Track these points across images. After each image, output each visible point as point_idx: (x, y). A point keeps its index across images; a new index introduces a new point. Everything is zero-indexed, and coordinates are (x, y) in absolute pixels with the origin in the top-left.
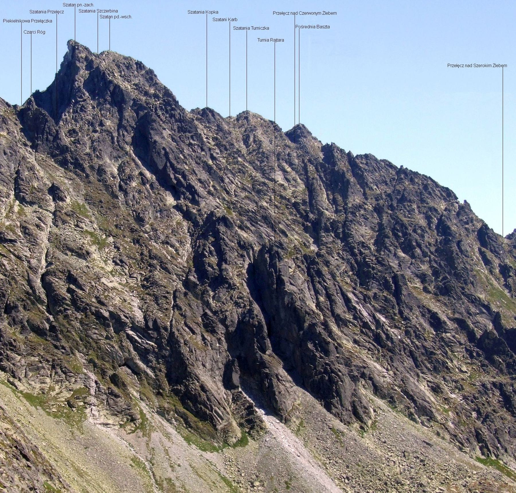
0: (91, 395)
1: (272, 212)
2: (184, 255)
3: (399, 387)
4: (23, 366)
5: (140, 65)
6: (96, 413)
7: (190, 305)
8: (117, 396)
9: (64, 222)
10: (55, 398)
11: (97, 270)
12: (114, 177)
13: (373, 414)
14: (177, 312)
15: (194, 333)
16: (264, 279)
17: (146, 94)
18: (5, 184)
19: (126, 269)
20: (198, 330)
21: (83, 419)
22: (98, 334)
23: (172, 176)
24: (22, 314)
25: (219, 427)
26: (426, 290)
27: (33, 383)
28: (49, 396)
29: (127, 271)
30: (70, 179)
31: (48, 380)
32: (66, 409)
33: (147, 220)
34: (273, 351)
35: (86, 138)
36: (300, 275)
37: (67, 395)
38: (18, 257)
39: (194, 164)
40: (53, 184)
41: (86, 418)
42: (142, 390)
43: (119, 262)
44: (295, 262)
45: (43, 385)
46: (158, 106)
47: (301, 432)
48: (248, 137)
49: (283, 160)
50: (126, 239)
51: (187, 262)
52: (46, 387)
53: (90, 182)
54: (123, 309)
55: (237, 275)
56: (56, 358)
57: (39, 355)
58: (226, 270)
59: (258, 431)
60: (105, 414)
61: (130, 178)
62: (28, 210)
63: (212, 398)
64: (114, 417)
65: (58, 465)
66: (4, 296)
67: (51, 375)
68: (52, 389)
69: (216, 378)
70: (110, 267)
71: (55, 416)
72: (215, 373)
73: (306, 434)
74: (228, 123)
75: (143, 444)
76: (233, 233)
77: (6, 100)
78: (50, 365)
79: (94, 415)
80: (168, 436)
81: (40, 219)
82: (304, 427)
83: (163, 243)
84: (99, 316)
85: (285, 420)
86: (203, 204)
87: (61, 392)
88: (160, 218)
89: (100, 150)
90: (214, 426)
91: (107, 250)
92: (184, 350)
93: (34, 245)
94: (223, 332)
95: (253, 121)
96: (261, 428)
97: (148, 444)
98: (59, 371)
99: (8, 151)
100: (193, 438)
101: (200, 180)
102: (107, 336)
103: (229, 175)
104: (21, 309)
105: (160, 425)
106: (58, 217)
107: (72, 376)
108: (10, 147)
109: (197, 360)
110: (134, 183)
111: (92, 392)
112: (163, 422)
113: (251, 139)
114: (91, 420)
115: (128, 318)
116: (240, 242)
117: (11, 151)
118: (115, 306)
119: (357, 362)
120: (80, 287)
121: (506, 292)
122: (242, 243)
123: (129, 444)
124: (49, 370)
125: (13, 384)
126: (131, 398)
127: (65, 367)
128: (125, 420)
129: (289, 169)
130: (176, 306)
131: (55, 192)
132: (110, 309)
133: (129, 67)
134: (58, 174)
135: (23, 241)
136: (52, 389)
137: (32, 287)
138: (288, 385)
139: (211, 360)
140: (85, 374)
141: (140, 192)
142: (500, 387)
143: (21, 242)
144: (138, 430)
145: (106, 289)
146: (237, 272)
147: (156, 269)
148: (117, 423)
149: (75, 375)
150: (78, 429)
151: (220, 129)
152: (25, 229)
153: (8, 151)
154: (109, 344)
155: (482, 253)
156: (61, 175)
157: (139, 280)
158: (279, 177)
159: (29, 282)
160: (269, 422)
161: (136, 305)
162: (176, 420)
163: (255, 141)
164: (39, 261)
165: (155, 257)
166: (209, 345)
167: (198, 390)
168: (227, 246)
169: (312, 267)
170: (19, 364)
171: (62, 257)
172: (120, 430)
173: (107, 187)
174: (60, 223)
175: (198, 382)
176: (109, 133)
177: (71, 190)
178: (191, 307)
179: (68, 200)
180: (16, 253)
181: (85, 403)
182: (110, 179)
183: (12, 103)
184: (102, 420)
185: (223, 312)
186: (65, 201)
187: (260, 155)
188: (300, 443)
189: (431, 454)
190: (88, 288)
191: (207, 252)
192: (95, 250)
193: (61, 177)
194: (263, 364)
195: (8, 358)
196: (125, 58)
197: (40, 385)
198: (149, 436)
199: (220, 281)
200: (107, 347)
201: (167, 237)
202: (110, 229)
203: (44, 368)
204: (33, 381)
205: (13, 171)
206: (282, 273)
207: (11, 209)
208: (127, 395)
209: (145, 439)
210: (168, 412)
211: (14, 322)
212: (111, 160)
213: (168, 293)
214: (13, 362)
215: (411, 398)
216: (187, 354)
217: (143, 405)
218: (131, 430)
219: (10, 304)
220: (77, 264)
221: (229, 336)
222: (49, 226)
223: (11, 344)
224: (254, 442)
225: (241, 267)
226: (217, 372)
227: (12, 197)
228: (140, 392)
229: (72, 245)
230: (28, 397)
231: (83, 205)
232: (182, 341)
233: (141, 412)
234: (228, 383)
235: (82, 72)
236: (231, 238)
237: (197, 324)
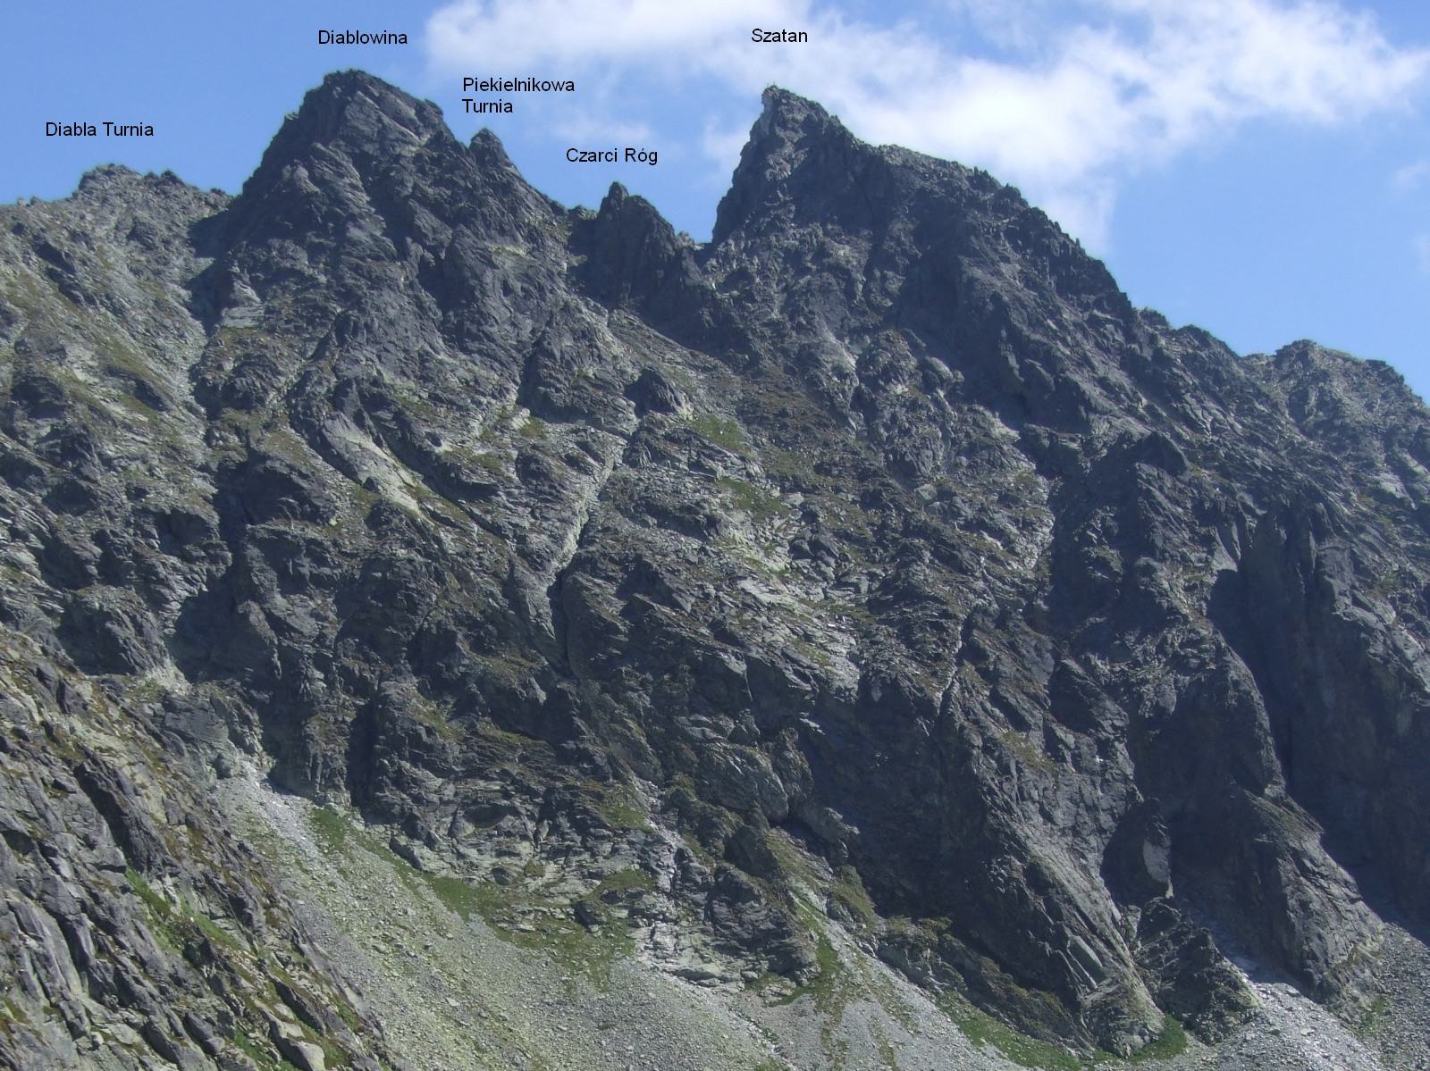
0: (657, 889)
2: (1031, 554)
4: (448, 803)
6: (668, 941)
7: (1013, 647)
8: (748, 895)
11: (729, 558)
12: (843, 375)
14: (969, 667)
15: (1019, 723)
18: (496, 365)
19: (828, 565)
20: (1036, 716)
21: (617, 954)
22: (708, 725)
23: (1012, 361)
24: (466, 662)
25: (1088, 999)
27: (473, 853)
28: (521, 889)
29: (830, 572)
30: (705, 370)
32: (568, 926)
33: (927, 470)
34: (1290, 790)
35: (774, 288)
36: (1411, 638)
37: (576, 886)
40: (643, 371)
41: (629, 948)
42: (839, 888)
43: (808, 551)
44: (1395, 608)
45: (507, 859)
46: (1003, 228)
47: (1375, 1028)
48: (1304, 397)
49: (1401, 445)
50: (842, 496)
51: (1037, 569)
52: (513, 865)
53: (759, 373)
54: (795, 656)
55: (1186, 589)
56: (559, 784)
57: (504, 774)
58: (1149, 571)
59: (1219, 1017)
60: (698, 944)
61: (891, 373)
62: (555, 432)
63: (1065, 908)
64: (726, 958)
65: (486, 1059)
66: (413, 608)
67: (536, 834)
68: (532, 871)
69: (1089, 856)
70: (780, 562)
71: (526, 940)
72: (1087, 842)
73: (1391, 1033)
74: (1250, 369)
75: (812, 1032)
76: (1182, 482)
77: (552, 197)
78: (537, 804)
79: (657, 946)
80: (904, 1014)
81: (583, 446)
82: (1388, 1013)
83: (968, 526)
84: (710, 671)
85: (1322, 993)
86: (1101, 428)
87: (562, 879)
88: (969, 467)
89: (812, 312)
90: (1073, 1005)
91: (777, 523)
92: (983, 767)
93: (548, 501)
94: (1118, 723)
96: (1234, 1007)
97: (828, 1032)
98: (564, 822)
99: (519, 285)
100: (995, 1027)
101: (1103, 382)
102: (737, 730)
103: (1211, 405)
104: (463, 646)
105: (879, 984)
107: (603, 837)
108: (526, 275)
109: (1022, 796)
110: (900, 387)
111: (664, 881)
112: (894, 978)
113: (1313, 400)
114: (646, 959)
115: (805, 678)
116: (1201, 502)
117: (526, 285)
120: (669, 599)
122: (1207, 505)
123: (765, 1031)
124: (531, 817)
125: (407, 854)
126: (790, 902)
127: (586, 811)
128: (765, 965)
130: (973, 653)
132: (754, 654)
134: (668, 356)
135: (516, 491)
136: (532, 871)
137: (518, 603)
138: (1335, 890)
139: (1071, 800)
140: (648, 832)
143: (509, 494)
144: (807, 996)
147: (921, 558)
148: (736, 975)
149: (616, 835)
150: (594, 978)
152: (529, 468)
153: (517, 286)
154: (741, 754)
156: (679, 360)
157: (864, 588)
159: (512, 587)
160: (1267, 998)
161: (845, 651)
162: (941, 975)
163: (1321, 404)
164: (558, 540)
166: (1069, 758)
167: (1017, 880)
168: (1158, 513)
170: (435, 798)
171: (626, 527)
172: (743, 995)
174: (644, 459)
175: (1022, 859)
176: (840, 271)
177: (701, 392)
178: (1019, 653)
179: (685, 410)
180: (489, 518)
181: (634, 912)
182: (829, 378)
183: (568, 204)
184: (684, 962)
185: (1133, 685)
186: (674, 410)
187: (1335, 435)
190: (693, 600)
191: (1095, 531)
192: (743, 523)
193: (678, 363)
194: (1254, 822)
195: (400, 781)
197: (495, 860)
198: (838, 1009)
200: (735, 761)
201: (980, 510)
202: (798, 473)
203: (515, 812)
204: (473, 846)
205: (526, 334)
206: (1327, 569)
207: (502, 423)
208: (783, 894)
209: (823, 1017)
210: (915, 950)
211: (435, 687)
212: (840, 337)
213: (945, 615)
214: (415, 791)
216: (992, 780)
218: (779, 994)
219: (430, 628)
220: (664, 544)
221: (1136, 734)
222: (610, 464)
223: (415, 739)
224: (1205, 1047)
225: (1200, 569)
226: (1093, 841)
227: (513, 397)
228: (829, 895)
230: (444, 888)
231: (730, 427)
232: (978, 741)
233: (825, 945)
234: (1123, 876)
235: (788, 149)
236: (1175, 494)
237: (1034, 698)
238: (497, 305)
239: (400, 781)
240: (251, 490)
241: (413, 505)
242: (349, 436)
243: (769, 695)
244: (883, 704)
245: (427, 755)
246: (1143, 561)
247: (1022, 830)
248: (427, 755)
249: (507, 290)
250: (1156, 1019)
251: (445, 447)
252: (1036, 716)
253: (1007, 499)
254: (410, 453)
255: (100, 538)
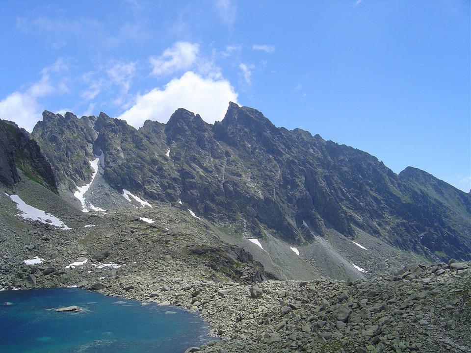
1: (311, 161)
3: (366, 223)
5: (257, 111)
7: (282, 192)
9: (231, 164)
10: (231, 229)
12: (249, 148)
13: (356, 233)
15: (284, 203)
16: (311, 184)
17: (260, 119)
26: (371, 190)
31: (227, 223)
38: (214, 177)
39: (279, 143)
43: (253, 178)
61: (255, 148)
62: (217, 160)
80: (275, 242)
81: (221, 163)
85: (322, 236)
95: (300, 132)
101: (282, 148)
106: (229, 163)
118: (252, 193)
119: (349, 214)
121: (400, 193)
129: (315, 148)
131: (227, 154)
133: (252, 112)
137: (220, 188)
141: (259, 153)
142: (403, 224)
145: (249, 187)
146: (301, 180)
151: (287, 134)
155: (390, 179)
158: (312, 151)
159: (218, 186)
160: (317, 238)
164: (222, 178)
165: (268, 176)
169: (326, 178)
171: (230, 176)
173: (247, 152)
188: (329, 244)
189: (381, 248)
195: (211, 215)
196: (251, 109)
199: (295, 186)
207: (210, 160)
208: (259, 227)
215: (371, 228)
217: (265, 231)
229: (235, 172)
238: (206, 143)
239: (211, 215)
240: (185, 174)
241: (203, 174)
242: (194, 165)
243: (252, 200)
244: (267, 201)
245: (213, 211)
246: (294, 178)
247: (286, 218)
248: (213, 211)
249: (207, 140)
250: (304, 241)
251: (205, 165)
252: (286, 202)
253: (274, 167)
254: (201, 166)
255: (167, 182)
